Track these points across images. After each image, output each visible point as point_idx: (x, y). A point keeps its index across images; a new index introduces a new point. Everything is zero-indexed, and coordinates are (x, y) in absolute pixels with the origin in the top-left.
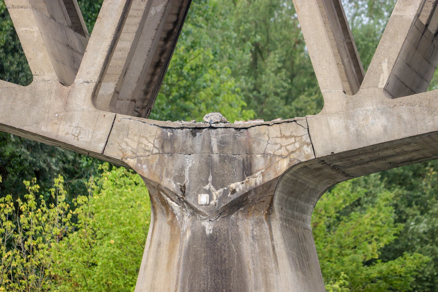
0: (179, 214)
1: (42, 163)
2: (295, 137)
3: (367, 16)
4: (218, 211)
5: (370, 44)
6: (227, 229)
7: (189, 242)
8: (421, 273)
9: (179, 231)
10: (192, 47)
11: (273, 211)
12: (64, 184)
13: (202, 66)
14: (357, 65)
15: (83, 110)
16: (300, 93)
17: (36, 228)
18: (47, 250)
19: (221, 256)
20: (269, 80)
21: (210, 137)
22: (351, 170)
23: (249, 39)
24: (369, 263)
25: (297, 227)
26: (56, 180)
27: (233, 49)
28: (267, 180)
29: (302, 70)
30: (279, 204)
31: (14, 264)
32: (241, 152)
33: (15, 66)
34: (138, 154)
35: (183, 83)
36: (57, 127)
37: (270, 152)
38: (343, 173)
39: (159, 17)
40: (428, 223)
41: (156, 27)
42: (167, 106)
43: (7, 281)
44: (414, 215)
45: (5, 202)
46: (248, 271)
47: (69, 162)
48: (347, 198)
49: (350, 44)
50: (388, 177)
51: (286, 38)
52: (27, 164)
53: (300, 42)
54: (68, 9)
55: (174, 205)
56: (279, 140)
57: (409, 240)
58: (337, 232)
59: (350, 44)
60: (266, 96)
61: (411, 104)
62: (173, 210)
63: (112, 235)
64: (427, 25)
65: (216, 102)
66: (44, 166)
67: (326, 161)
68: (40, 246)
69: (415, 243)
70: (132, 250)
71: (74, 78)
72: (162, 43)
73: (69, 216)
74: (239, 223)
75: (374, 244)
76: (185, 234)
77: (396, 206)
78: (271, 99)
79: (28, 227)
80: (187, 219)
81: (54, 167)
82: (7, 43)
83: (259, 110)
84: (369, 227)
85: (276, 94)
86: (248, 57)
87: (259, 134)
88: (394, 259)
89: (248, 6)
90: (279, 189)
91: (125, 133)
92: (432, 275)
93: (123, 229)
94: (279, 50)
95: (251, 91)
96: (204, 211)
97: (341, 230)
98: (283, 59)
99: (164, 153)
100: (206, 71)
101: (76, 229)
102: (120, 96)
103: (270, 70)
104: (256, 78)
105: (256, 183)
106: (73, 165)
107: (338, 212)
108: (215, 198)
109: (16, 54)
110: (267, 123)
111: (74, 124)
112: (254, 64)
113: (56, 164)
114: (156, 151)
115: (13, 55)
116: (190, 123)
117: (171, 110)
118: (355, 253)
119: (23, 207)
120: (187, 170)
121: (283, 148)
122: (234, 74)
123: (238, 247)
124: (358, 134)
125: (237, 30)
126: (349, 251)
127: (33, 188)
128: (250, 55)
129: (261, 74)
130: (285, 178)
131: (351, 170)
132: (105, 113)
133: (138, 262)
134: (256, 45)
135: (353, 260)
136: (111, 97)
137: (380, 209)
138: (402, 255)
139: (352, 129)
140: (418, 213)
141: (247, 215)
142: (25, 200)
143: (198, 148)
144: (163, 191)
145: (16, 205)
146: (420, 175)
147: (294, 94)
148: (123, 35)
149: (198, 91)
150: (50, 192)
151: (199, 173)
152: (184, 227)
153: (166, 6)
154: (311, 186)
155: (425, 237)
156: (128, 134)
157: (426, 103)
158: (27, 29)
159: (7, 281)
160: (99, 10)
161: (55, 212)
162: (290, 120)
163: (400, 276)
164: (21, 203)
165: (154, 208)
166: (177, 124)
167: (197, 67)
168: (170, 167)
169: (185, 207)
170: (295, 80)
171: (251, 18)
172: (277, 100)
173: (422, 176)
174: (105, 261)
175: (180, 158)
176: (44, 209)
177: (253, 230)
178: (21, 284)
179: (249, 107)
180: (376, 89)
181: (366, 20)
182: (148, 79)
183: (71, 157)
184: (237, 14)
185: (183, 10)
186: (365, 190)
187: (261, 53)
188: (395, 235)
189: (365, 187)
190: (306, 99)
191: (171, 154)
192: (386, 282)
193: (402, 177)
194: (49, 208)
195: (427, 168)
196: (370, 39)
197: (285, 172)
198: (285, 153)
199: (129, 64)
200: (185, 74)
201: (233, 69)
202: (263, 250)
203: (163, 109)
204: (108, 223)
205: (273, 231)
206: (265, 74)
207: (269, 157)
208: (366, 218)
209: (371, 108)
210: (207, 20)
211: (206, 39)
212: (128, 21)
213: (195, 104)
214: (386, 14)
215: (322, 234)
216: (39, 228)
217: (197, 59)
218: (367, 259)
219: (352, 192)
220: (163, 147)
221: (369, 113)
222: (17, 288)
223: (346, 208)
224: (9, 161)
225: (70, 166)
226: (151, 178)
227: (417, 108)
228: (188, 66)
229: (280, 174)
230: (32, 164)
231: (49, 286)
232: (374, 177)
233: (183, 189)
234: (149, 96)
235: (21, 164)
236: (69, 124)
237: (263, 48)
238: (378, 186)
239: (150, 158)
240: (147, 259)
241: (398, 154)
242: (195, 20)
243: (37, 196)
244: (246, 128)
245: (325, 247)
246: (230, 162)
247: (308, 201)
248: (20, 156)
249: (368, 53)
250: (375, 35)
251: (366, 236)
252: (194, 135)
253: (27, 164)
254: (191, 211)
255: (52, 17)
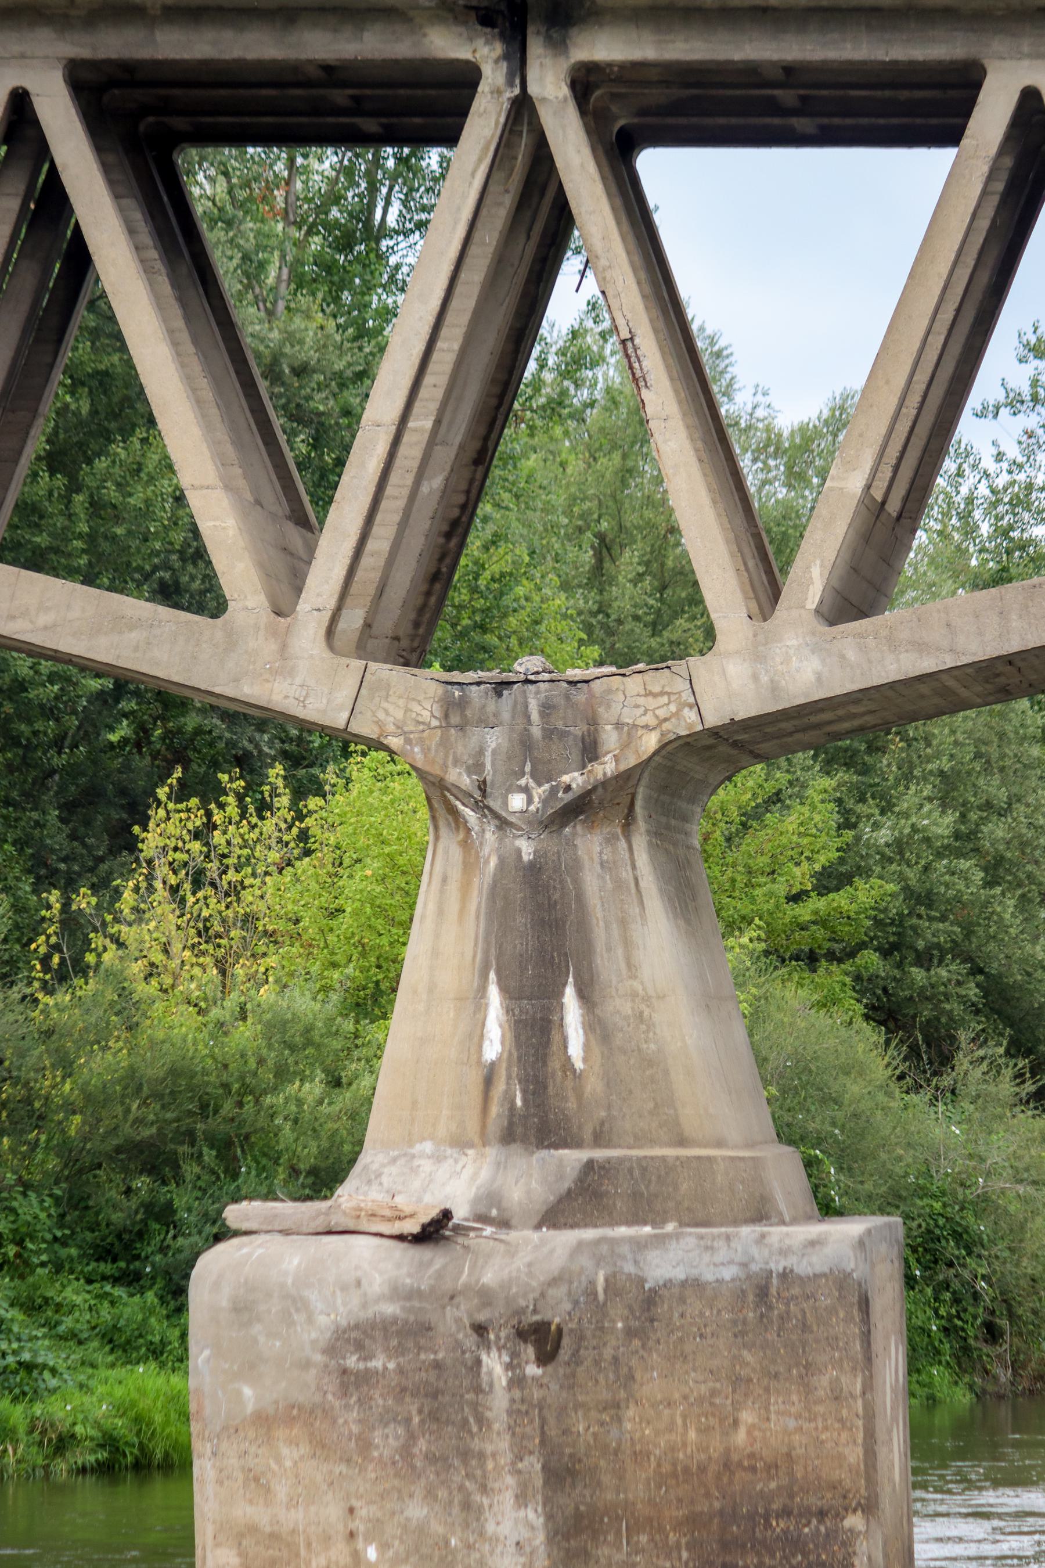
0: (477, 828)
1: (246, 743)
2: (669, 694)
3: (784, 485)
4: (541, 822)
5: (790, 531)
6: (558, 852)
7: (495, 875)
8: (880, 911)
9: (478, 857)
10: (494, 543)
11: (634, 819)
12: (285, 778)
13: (511, 574)
14: (769, 571)
15: (311, 657)
16: (676, 615)
17: (239, 852)
18: (260, 888)
19: (549, 898)
20: (623, 594)
21: (526, 698)
22: (765, 747)
23: (589, 528)
24: (795, 898)
25: (675, 844)
26: (272, 772)
27: (563, 544)
28: (623, 767)
29: (678, 577)
30: (644, 808)
31: (205, 913)
32: (579, 722)
33: (198, 582)
34: (406, 729)
35: (479, 604)
36: (268, 686)
37: (627, 720)
38: (751, 752)
39: (436, 497)
40: (892, 829)
41: (431, 514)
42: (453, 643)
43: (196, 940)
44: (869, 817)
45: (188, 810)
46: (594, 921)
47: (291, 740)
48: (759, 791)
49: (757, 536)
50: (826, 753)
51: (652, 526)
52: (221, 745)
53: (674, 530)
54: (284, 488)
55: (469, 813)
56: (641, 701)
57: (862, 857)
58: (743, 848)
59: (757, 536)
60: (620, 622)
61: (861, 636)
62: (466, 822)
63: (368, 861)
64: (884, 503)
65: (537, 635)
66: (250, 747)
67: (722, 733)
68: (247, 882)
69: (871, 862)
70: (403, 885)
71: (297, 603)
72: (442, 540)
73: (295, 831)
74: (578, 842)
75: (805, 865)
76: (487, 862)
77: (839, 801)
78: (627, 627)
79: (226, 851)
80: (490, 836)
81: (266, 749)
82: (186, 544)
83: (608, 646)
84: (795, 838)
85: (636, 618)
86: (588, 557)
87: (609, 691)
88: (838, 890)
89: (586, 471)
90: (643, 782)
91: (384, 693)
92: (900, 914)
93: (387, 850)
94: (639, 545)
95: (594, 614)
96: (519, 823)
97: (748, 845)
98: (645, 559)
99: (449, 726)
100: (518, 583)
101: (308, 853)
102: (375, 631)
103: (625, 577)
104: (601, 592)
105: (605, 774)
106: (298, 745)
107: (744, 815)
108: (536, 799)
109: (200, 562)
110: (622, 671)
111: (298, 681)
112: (598, 566)
113: (271, 744)
114: (435, 723)
115: (195, 564)
116: (494, 675)
117: (461, 649)
118: (774, 881)
119: (218, 818)
120: (488, 754)
121: (650, 714)
122: (566, 586)
123: (577, 882)
124: (774, 688)
125: (568, 513)
126: (763, 879)
127: (234, 786)
128: (591, 553)
129: (610, 585)
130: (653, 764)
131: (765, 747)
132: (347, 661)
133: (412, 907)
134: (601, 537)
135: (771, 894)
136: (358, 634)
137: (813, 808)
138: (851, 884)
139: (764, 679)
140: (877, 812)
141: (591, 825)
142: (222, 806)
143: (506, 716)
144: (449, 791)
145: (209, 814)
146: (878, 749)
147: (666, 618)
148: (376, 530)
149: (505, 615)
150: (262, 793)
151: (509, 758)
152: (486, 850)
153: (447, 480)
154: (696, 776)
155: (887, 851)
156: (387, 696)
157: (884, 633)
158: (217, 523)
159: (196, 940)
160: (337, 483)
161: (269, 826)
162: (660, 665)
163: (849, 918)
164: (216, 811)
165: (434, 818)
166: (470, 676)
167: (503, 575)
168: (460, 749)
169: (485, 816)
170: (669, 592)
171: (591, 492)
172: (638, 627)
173: (883, 750)
174: (358, 904)
175: (475, 735)
176: (254, 820)
177: (601, 853)
178: (219, 946)
179: (591, 641)
180: (802, 611)
181: (782, 493)
182: (420, 601)
183: (294, 732)
184: (568, 485)
185: (477, 483)
186: (789, 777)
187: (608, 550)
188: (838, 850)
189: (788, 771)
190: (687, 625)
191: (461, 728)
192: (825, 928)
193: (849, 754)
194: (262, 818)
195: (890, 737)
196: (791, 523)
197: (654, 754)
198: (652, 722)
199: (387, 577)
200: (483, 588)
201: (564, 577)
202: (619, 885)
203: (446, 648)
204: (362, 841)
205: (636, 853)
206: (617, 585)
207: (626, 728)
208: (791, 822)
209: (793, 642)
210: (517, 497)
211: (517, 529)
212: (384, 504)
213: (500, 638)
214: (815, 480)
215: (718, 851)
216: (246, 852)
217: (503, 562)
218: (794, 892)
219: (766, 780)
220: (446, 716)
221: (792, 652)
222: (211, 951)
223: (757, 806)
224: (192, 740)
225: (294, 748)
226: (427, 768)
227: (871, 641)
228: (487, 574)
229: (645, 757)
230: (231, 744)
231: (264, 949)
232: (802, 758)
233: (482, 786)
234: (421, 631)
235: (211, 744)
236: (289, 681)
237: (613, 541)
238: (809, 768)
239: (425, 734)
240: (425, 904)
241: (840, 719)
242: (497, 498)
243: (240, 798)
244: (587, 682)
245: (723, 872)
246: (560, 739)
247: (692, 800)
248: (210, 732)
249: (787, 546)
250: (798, 517)
251: (790, 853)
252: (499, 695)
253: (221, 745)
254: (497, 822)
255: (258, 502)
